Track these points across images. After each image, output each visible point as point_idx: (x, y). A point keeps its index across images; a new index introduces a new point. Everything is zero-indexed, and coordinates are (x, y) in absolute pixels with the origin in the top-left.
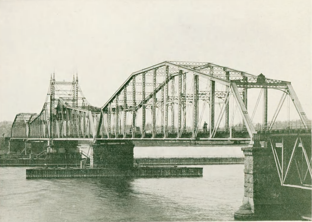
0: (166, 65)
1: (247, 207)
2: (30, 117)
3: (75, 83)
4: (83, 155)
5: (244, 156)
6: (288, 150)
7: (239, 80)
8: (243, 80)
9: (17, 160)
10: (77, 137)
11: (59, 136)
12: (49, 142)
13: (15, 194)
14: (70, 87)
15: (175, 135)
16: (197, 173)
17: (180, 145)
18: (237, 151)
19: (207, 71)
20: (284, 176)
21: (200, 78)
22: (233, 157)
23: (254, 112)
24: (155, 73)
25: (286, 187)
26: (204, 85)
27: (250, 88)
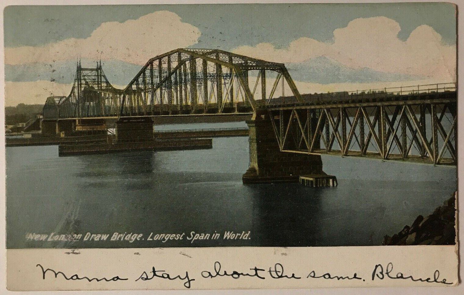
0: (179, 52)
1: (252, 170)
2: (59, 100)
3: (99, 69)
4: (108, 132)
5: (248, 128)
6: (286, 122)
7: (242, 63)
8: (244, 63)
9: (148, 125)
10: (103, 116)
11: (131, 114)
12: (77, 121)
13: (414, 86)
14: (94, 73)
15: (232, 110)
16: (208, 146)
17: (390, 94)
18: (242, 125)
19: (213, 57)
20: (282, 144)
21: (209, 63)
22: (389, 91)
23: (255, 89)
24: (169, 58)
25: (284, 152)
26: (211, 68)
27: (251, 69)
